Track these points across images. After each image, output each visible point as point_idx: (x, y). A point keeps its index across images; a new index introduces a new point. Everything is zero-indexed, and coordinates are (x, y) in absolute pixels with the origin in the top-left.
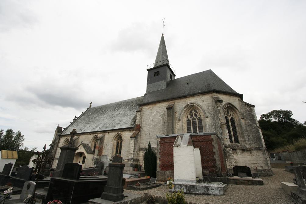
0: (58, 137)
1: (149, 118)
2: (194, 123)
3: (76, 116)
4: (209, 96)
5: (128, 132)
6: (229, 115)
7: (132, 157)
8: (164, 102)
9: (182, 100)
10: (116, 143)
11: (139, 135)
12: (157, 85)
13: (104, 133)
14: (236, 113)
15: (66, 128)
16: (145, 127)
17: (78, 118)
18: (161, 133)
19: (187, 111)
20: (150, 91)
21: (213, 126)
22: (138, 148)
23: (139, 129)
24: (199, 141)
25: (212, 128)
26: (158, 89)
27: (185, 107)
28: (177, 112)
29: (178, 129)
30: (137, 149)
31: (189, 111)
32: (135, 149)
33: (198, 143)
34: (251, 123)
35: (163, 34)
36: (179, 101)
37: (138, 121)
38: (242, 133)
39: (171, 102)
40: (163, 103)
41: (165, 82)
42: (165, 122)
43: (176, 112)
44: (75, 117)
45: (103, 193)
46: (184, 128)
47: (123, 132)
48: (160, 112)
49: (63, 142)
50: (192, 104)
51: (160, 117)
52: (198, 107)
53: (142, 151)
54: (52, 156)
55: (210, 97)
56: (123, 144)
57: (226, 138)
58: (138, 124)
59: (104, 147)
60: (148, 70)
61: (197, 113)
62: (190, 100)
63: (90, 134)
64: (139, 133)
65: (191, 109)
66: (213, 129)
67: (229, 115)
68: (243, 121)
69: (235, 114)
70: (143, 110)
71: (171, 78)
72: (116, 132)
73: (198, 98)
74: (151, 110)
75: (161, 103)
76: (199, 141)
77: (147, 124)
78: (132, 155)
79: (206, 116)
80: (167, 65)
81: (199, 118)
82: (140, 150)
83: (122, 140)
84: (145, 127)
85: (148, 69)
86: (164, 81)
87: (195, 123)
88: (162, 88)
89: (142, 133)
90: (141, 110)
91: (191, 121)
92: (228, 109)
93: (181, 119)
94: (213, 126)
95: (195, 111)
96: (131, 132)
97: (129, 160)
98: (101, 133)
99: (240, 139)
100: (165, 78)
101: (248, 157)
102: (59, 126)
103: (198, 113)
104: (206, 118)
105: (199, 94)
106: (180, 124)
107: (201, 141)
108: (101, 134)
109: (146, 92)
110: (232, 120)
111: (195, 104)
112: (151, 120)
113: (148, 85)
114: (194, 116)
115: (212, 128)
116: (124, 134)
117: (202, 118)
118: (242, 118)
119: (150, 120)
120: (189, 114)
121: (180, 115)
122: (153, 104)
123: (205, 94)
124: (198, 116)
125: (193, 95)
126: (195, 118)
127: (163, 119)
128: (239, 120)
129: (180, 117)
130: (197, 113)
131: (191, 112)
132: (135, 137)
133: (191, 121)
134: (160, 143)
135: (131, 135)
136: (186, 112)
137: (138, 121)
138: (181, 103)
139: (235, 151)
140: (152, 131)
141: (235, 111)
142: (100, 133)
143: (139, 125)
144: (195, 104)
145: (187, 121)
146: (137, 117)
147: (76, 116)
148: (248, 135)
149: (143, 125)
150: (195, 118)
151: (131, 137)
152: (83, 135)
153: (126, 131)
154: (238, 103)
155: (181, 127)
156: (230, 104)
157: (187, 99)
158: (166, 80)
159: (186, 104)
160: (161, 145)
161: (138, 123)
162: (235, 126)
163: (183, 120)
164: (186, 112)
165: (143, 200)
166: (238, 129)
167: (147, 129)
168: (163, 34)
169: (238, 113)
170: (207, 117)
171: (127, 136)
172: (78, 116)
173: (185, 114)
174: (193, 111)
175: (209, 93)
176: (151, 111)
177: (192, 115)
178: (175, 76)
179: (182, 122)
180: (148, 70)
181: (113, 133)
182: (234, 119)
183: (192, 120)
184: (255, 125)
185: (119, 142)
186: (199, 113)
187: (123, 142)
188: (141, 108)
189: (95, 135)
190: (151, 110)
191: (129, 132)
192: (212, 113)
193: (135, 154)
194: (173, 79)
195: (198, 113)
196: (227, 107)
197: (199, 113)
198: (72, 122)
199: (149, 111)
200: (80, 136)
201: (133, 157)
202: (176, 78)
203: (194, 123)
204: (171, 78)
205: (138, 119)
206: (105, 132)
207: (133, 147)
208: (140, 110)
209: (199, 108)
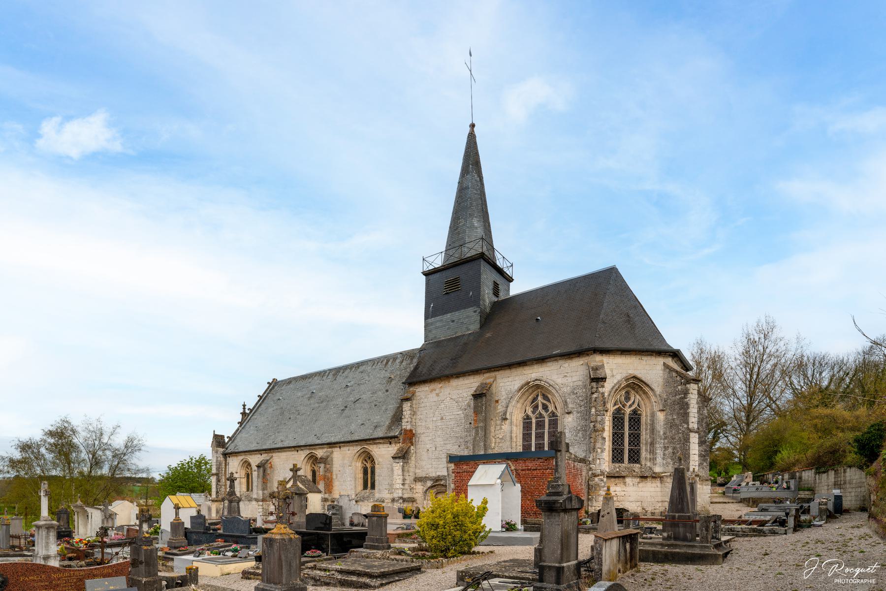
0: (221, 456)
1: (434, 413)
2: (540, 425)
3: (244, 406)
4: (581, 362)
5: (385, 446)
6: (628, 404)
7: (400, 495)
8: (469, 375)
9: (513, 370)
10: (360, 468)
11: (412, 451)
12: (453, 321)
13: (330, 448)
14: (649, 398)
15: (233, 436)
16: (424, 433)
17: (251, 410)
18: (462, 447)
19: (525, 397)
20: (435, 337)
21: (581, 433)
22: (412, 478)
23: (411, 439)
24: (528, 470)
25: (577, 436)
26: (456, 333)
27: (520, 390)
28: (500, 402)
29: (502, 439)
30: (409, 479)
31: (530, 397)
32: (404, 480)
33: (527, 472)
34: (677, 422)
35: (473, 126)
36: (507, 372)
37: (407, 422)
38: (652, 444)
39: (487, 375)
40: (465, 378)
41: (475, 312)
42: (470, 423)
43: (497, 401)
44: (244, 409)
45: (365, 543)
46: (514, 435)
47: (375, 446)
48: (460, 399)
49: (236, 466)
50: (538, 382)
51: (458, 413)
52: (550, 388)
53: (420, 483)
54: (238, 497)
55: (582, 365)
56: (377, 471)
57: (599, 459)
58: (409, 428)
59: (334, 477)
60: (427, 274)
61: (549, 400)
62: (533, 373)
63: (298, 451)
64: (412, 447)
65: (536, 392)
66: (578, 439)
67: (628, 404)
68: (661, 416)
69: (646, 401)
70: (417, 394)
71: (496, 292)
72: (357, 445)
73: (552, 368)
74: (438, 395)
75: (461, 379)
76: (528, 470)
77: (428, 428)
78: (400, 491)
79: (566, 411)
80: (486, 259)
81: (553, 414)
82: (415, 481)
83: (373, 461)
84: (424, 433)
85: (426, 269)
86: (471, 309)
87: (540, 425)
88: (469, 330)
89: (418, 447)
90: (413, 395)
91: (534, 421)
92: (629, 389)
93: (508, 416)
94: (581, 433)
95: (545, 397)
96: (393, 445)
97: (393, 500)
98: (323, 448)
99: (644, 454)
100: (476, 301)
101: (652, 489)
102: (216, 433)
103: (552, 403)
104: (567, 415)
105: (558, 358)
106: (506, 427)
107: (533, 470)
108: (325, 450)
109: (423, 342)
110: (635, 419)
111: (545, 382)
112: (439, 418)
113: (430, 321)
114: (540, 408)
115: (577, 436)
116: (378, 449)
117: (559, 415)
118: (661, 408)
119: (435, 419)
120: (529, 404)
121: (507, 407)
122: (442, 381)
123: (572, 356)
124: (551, 408)
125: (542, 360)
126: (543, 413)
127: (466, 416)
128: (653, 415)
129: (505, 413)
130: (549, 400)
131: (535, 399)
132: (403, 456)
133: (534, 421)
134: (453, 473)
135: (395, 452)
136: (522, 401)
137: (407, 422)
138: (510, 379)
139: (621, 479)
140: (442, 443)
141: (645, 393)
142: (320, 448)
143: (411, 431)
144: (545, 382)
145: (524, 419)
146: (404, 413)
147: (244, 406)
148: (665, 447)
149: (419, 430)
150: (543, 413)
151: (394, 458)
152: (279, 452)
153: (380, 443)
154: (661, 372)
155: (508, 435)
156: (635, 377)
157: (526, 368)
158: (478, 306)
159: (523, 382)
160: (456, 476)
161: (406, 425)
162: (614, 434)
163: (514, 418)
164: (522, 401)
165: (331, 376)
166: (646, 434)
167: (430, 438)
168: (473, 126)
169: (653, 399)
170: (569, 413)
171: (383, 453)
172: (250, 405)
173: (519, 405)
174: (540, 398)
175: (583, 354)
176: (436, 399)
177: (536, 407)
178: (510, 280)
179: (511, 423)
180: (427, 274)
181: (351, 448)
182: (639, 412)
183: (537, 418)
184: (686, 426)
185: (369, 465)
186: (554, 403)
187: (377, 466)
188: (411, 389)
189: (308, 452)
190: (438, 395)
191: (388, 445)
192: (582, 404)
193: (407, 489)
194: (502, 296)
195: (550, 402)
196: (627, 386)
197: (554, 403)
198: (240, 421)
199: (433, 397)
200: (274, 455)
201: (403, 494)
202: (515, 289)
203: (540, 425)
204: (496, 292)
205: (407, 417)
206: (331, 445)
207: (401, 477)
208: (409, 395)
209: (554, 391)
